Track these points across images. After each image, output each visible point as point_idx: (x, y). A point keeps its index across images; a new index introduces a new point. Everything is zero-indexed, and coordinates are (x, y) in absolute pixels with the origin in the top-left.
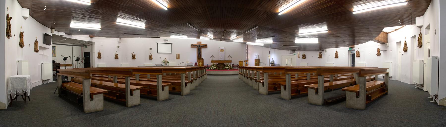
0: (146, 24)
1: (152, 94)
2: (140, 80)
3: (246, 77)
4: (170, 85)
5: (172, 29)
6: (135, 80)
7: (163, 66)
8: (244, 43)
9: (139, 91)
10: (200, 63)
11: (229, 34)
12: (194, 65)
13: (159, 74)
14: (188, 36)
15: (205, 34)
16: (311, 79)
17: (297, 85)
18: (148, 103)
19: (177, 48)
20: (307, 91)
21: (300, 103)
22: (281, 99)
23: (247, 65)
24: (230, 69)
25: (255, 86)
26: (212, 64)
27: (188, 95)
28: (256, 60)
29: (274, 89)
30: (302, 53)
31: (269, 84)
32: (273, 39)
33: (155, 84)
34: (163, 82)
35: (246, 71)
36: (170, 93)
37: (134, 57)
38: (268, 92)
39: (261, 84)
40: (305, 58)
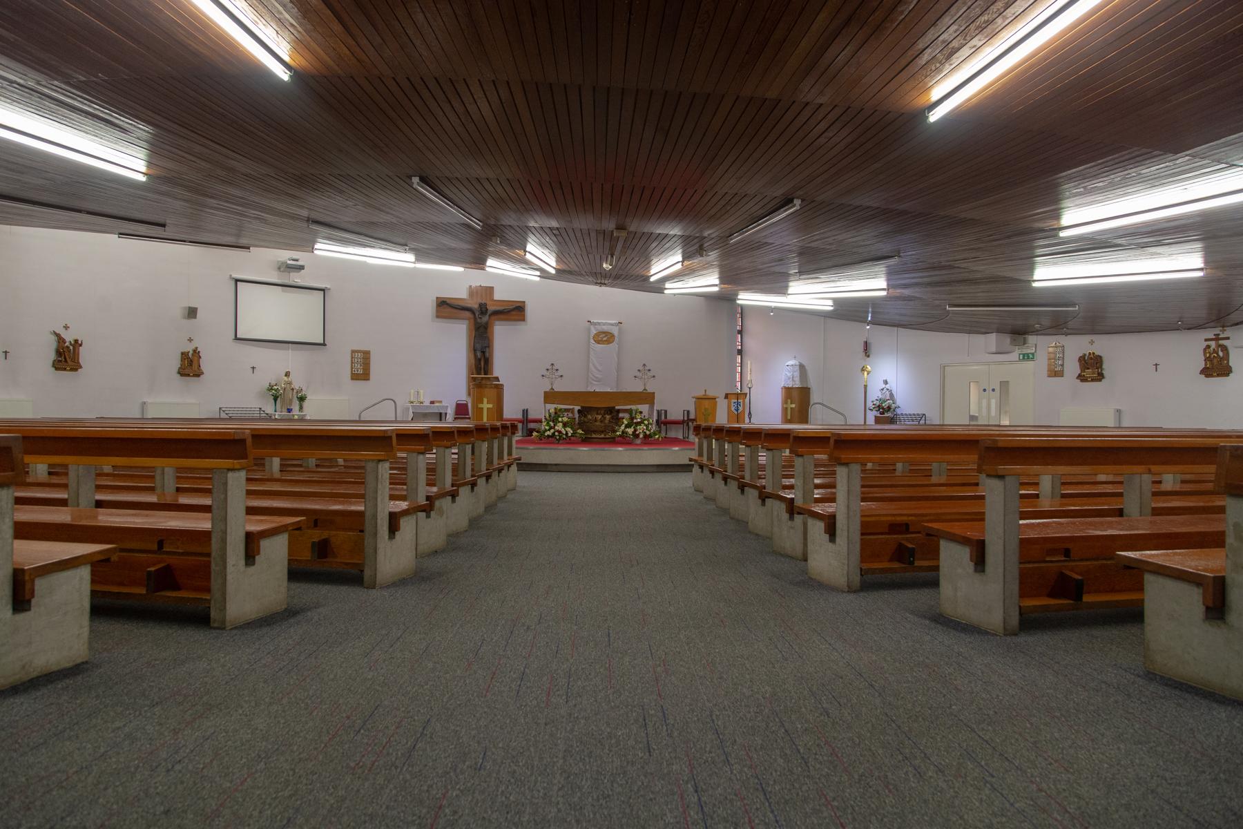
0: (156, 152)
1: (177, 587)
2: (99, 504)
3: (733, 485)
4: (298, 527)
5: (324, 204)
6: (63, 503)
7: (269, 418)
8: (723, 301)
9: (85, 572)
10: (486, 406)
11: (645, 248)
12: (451, 412)
13: (228, 463)
14: (421, 255)
15: (510, 246)
16: (1157, 512)
17: (1064, 548)
18: (150, 647)
19: (351, 310)
20: (1141, 589)
21: (1075, 665)
22: (941, 620)
23: (739, 418)
24: (648, 440)
25: (787, 534)
26: (552, 408)
27: (401, 582)
28: (788, 392)
29: (899, 557)
30: (1076, 346)
31: (868, 529)
32: (890, 275)
33: (202, 523)
34: (251, 511)
35: (736, 455)
36: (296, 574)
37: (67, 357)
38: (863, 572)
39: (820, 526)
40: (1100, 377)
